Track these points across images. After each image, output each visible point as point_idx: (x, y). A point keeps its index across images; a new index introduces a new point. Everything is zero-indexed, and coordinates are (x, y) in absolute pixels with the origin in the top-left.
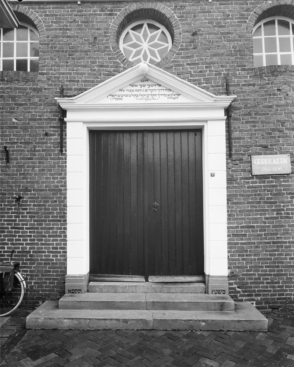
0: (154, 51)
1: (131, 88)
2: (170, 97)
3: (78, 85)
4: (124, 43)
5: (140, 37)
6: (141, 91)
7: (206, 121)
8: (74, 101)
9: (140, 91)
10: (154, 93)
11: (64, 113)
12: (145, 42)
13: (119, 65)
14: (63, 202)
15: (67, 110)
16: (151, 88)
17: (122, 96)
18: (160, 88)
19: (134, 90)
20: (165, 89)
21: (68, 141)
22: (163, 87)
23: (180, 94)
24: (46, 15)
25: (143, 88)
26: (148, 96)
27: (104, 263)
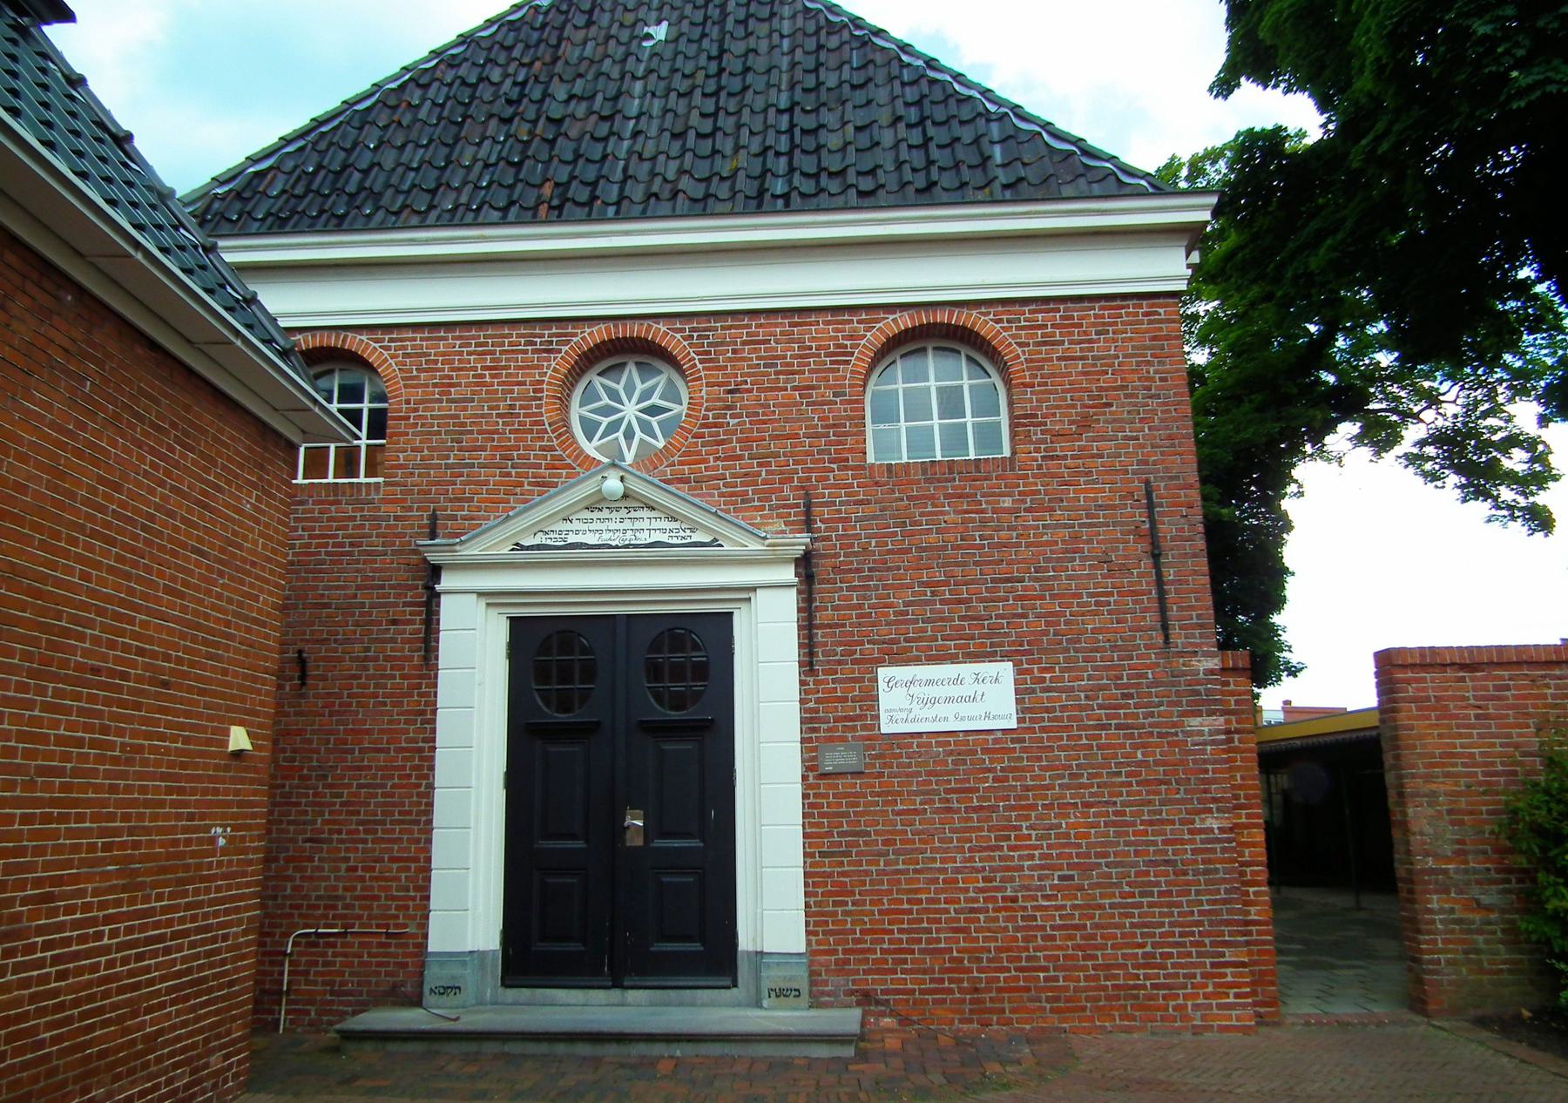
0: (649, 423)
1: (587, 514)
7: (754, 589)
11: (435, 571)
13: (564, 465)
14: (426, 777)
18: (653, 514)
21: (793, 629)
24: (406, 355)
27: (530, 951)
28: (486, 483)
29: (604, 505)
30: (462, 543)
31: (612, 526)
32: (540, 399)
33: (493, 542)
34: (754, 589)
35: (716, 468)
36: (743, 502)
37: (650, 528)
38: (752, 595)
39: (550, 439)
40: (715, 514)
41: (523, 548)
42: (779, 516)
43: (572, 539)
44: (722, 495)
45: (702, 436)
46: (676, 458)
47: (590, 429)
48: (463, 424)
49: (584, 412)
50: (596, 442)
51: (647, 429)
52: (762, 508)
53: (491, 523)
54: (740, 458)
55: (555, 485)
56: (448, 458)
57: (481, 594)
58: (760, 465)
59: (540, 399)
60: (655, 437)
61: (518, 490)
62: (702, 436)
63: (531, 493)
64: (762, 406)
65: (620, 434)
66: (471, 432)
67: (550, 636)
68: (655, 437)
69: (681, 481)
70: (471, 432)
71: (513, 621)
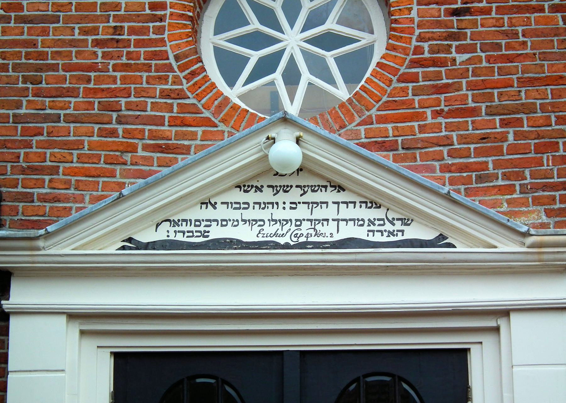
1: (239, 196)
2: (376, 228)
3: (54, 185)
4: (218, 31)
5: (312, 71)
6: (275, 206)
8: (41, 243)
9: (270, 206)
10: (319, 213)
12: (292, 26)
13: (189, 122)
15: (12, 271)
16: (310, 197)
17: (209, 223)
19: (251, 205)
20: (358, 200)
22: (351, 194)
23: (412, 217)
25: (281, 197)
26: (298, 223)
28: (78, 145)
29: (263, 182)
30: (48, 235)
31: (279, 214)
32: (161, 19)
33: (94, 237)
34: (505, 313)
35: (437, 127)
36: (480, 179)
37: (339, 219)
38: (502, 323)
39: (177, 81)
40: (447, 197)
41: (140, 246)
42: (537, 201)
43: (216, 233)
44: (446, 168)
45: (414, 78)
46: (374, 112)
47: (231, 66)
48: (42, 56)
49: (222, 40)
50: (365, 39)
51: (319, 68)
52: (510, 189)
53: (191, 158)
54: (474, 112)
55: (186, 150)
56: (19, 106)
57: (73, 316)
58: (505, 123)
59: (161, 19)
60: (331, 81)
61: (128, 157)
62: (414, 78)
63: (148, 161)
64: (506, 34)
65: (277, 76)
66: (54, 67)
67: (181, 382)
68: (331, 81)
69: (382, 146)
70: (54, 67)
71: (122, 360)
